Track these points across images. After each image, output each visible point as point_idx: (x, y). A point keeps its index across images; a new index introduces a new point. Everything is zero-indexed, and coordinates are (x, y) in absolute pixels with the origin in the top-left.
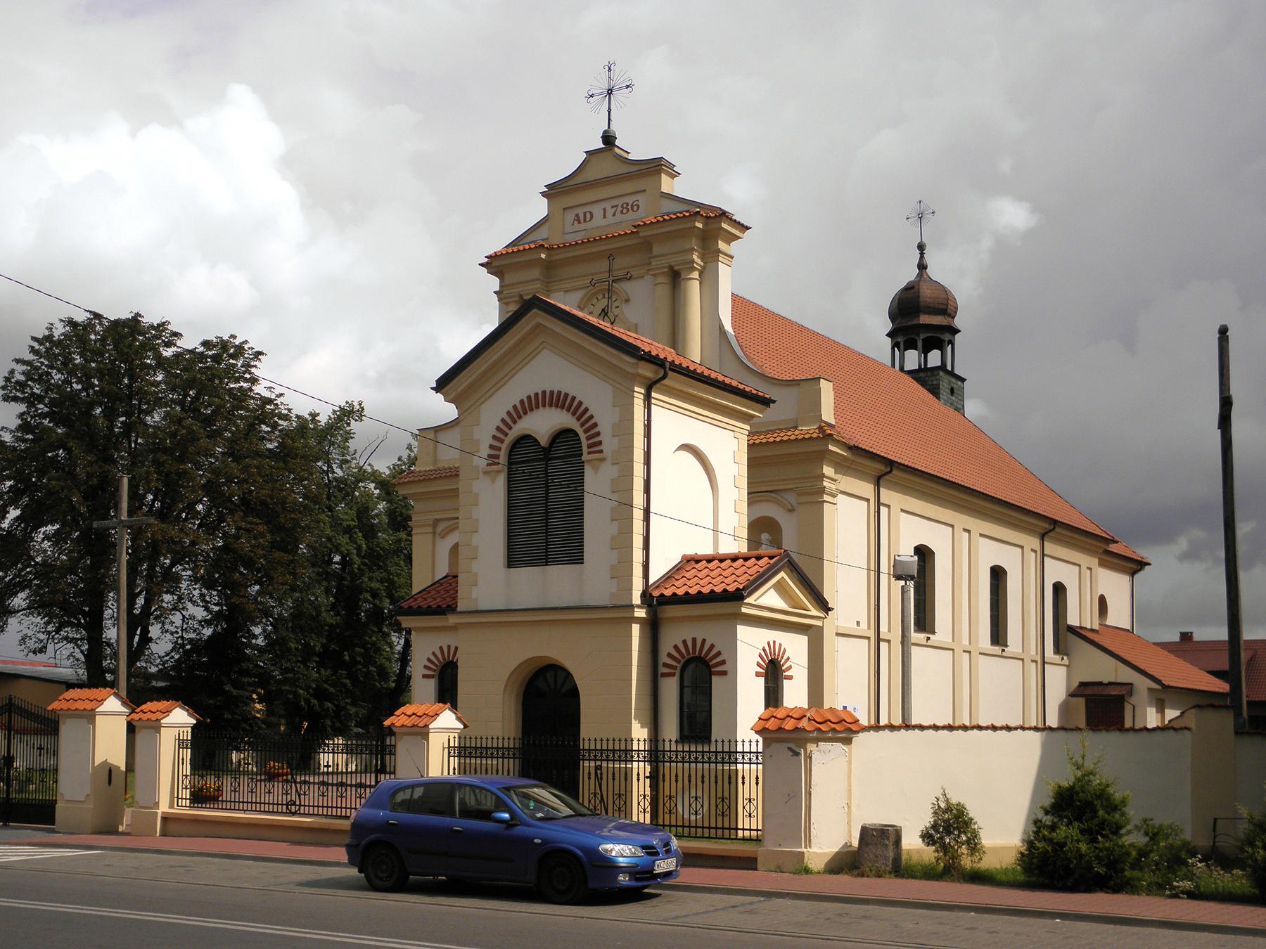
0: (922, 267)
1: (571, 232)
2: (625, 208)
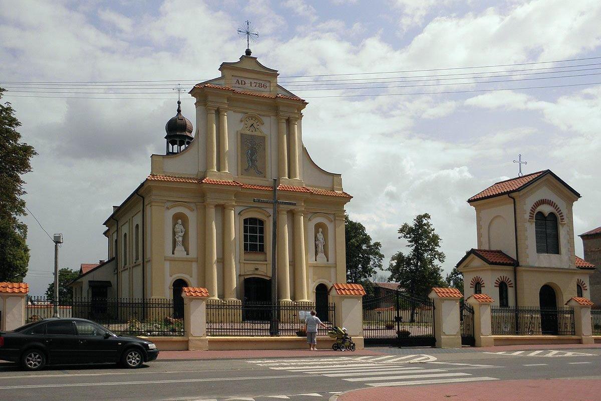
0: (179, 111)
1: (223, 84)
2: (260, 86)
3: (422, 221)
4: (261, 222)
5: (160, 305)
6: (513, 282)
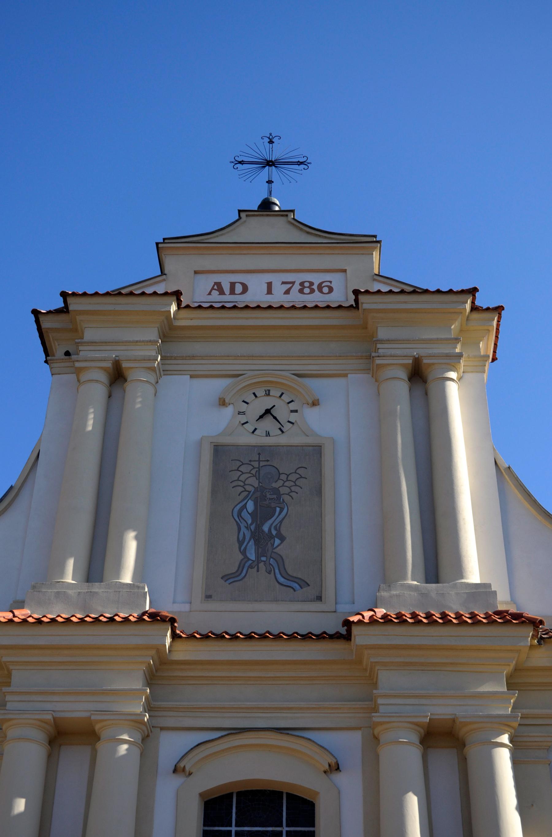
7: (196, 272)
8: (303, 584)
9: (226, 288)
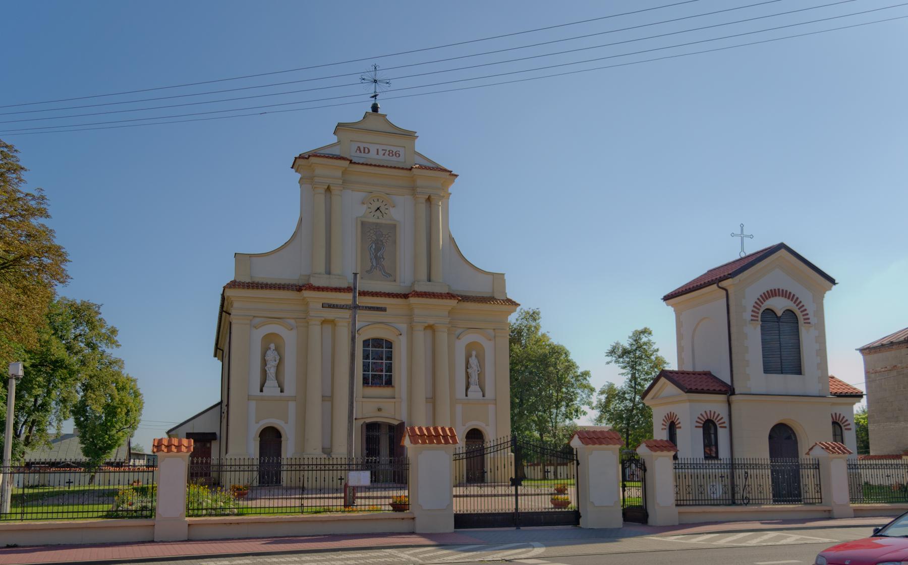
3: (640, 338)
4: (389, 345)
5: (233, 469)
6: (726, 419)
7: (429, 280)
8: (390, 275)
9: (362, 150)
